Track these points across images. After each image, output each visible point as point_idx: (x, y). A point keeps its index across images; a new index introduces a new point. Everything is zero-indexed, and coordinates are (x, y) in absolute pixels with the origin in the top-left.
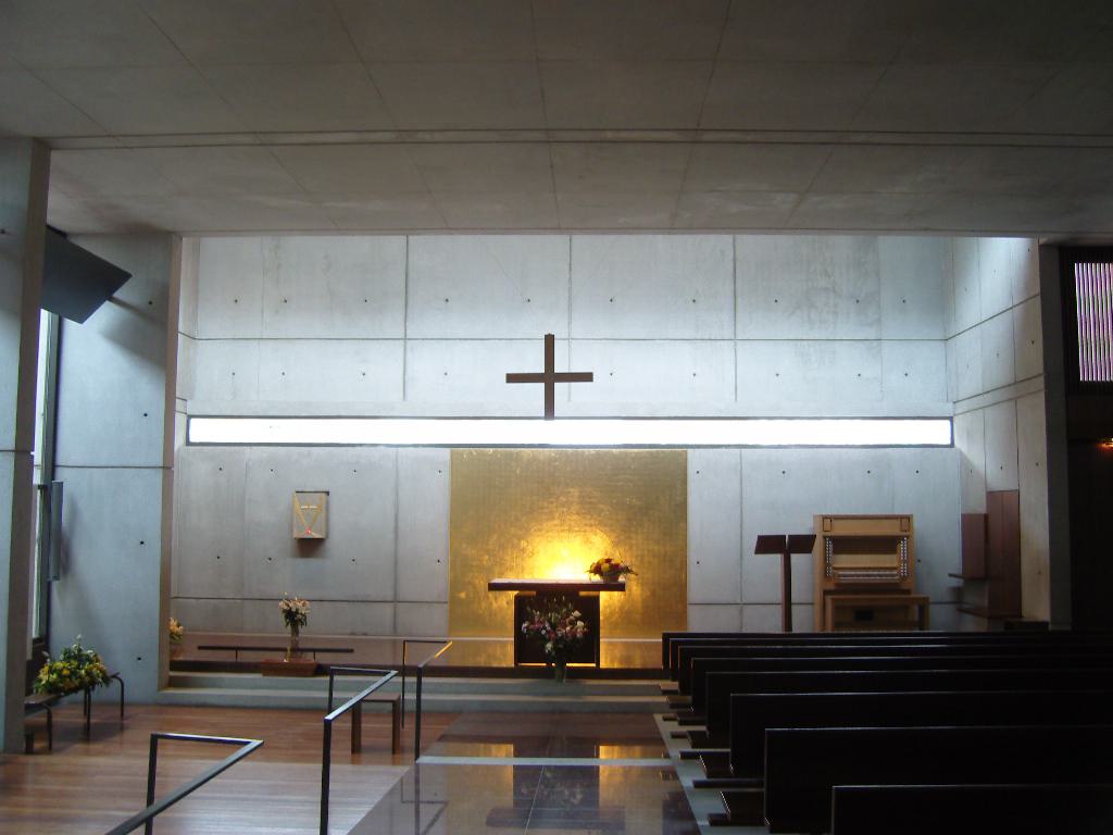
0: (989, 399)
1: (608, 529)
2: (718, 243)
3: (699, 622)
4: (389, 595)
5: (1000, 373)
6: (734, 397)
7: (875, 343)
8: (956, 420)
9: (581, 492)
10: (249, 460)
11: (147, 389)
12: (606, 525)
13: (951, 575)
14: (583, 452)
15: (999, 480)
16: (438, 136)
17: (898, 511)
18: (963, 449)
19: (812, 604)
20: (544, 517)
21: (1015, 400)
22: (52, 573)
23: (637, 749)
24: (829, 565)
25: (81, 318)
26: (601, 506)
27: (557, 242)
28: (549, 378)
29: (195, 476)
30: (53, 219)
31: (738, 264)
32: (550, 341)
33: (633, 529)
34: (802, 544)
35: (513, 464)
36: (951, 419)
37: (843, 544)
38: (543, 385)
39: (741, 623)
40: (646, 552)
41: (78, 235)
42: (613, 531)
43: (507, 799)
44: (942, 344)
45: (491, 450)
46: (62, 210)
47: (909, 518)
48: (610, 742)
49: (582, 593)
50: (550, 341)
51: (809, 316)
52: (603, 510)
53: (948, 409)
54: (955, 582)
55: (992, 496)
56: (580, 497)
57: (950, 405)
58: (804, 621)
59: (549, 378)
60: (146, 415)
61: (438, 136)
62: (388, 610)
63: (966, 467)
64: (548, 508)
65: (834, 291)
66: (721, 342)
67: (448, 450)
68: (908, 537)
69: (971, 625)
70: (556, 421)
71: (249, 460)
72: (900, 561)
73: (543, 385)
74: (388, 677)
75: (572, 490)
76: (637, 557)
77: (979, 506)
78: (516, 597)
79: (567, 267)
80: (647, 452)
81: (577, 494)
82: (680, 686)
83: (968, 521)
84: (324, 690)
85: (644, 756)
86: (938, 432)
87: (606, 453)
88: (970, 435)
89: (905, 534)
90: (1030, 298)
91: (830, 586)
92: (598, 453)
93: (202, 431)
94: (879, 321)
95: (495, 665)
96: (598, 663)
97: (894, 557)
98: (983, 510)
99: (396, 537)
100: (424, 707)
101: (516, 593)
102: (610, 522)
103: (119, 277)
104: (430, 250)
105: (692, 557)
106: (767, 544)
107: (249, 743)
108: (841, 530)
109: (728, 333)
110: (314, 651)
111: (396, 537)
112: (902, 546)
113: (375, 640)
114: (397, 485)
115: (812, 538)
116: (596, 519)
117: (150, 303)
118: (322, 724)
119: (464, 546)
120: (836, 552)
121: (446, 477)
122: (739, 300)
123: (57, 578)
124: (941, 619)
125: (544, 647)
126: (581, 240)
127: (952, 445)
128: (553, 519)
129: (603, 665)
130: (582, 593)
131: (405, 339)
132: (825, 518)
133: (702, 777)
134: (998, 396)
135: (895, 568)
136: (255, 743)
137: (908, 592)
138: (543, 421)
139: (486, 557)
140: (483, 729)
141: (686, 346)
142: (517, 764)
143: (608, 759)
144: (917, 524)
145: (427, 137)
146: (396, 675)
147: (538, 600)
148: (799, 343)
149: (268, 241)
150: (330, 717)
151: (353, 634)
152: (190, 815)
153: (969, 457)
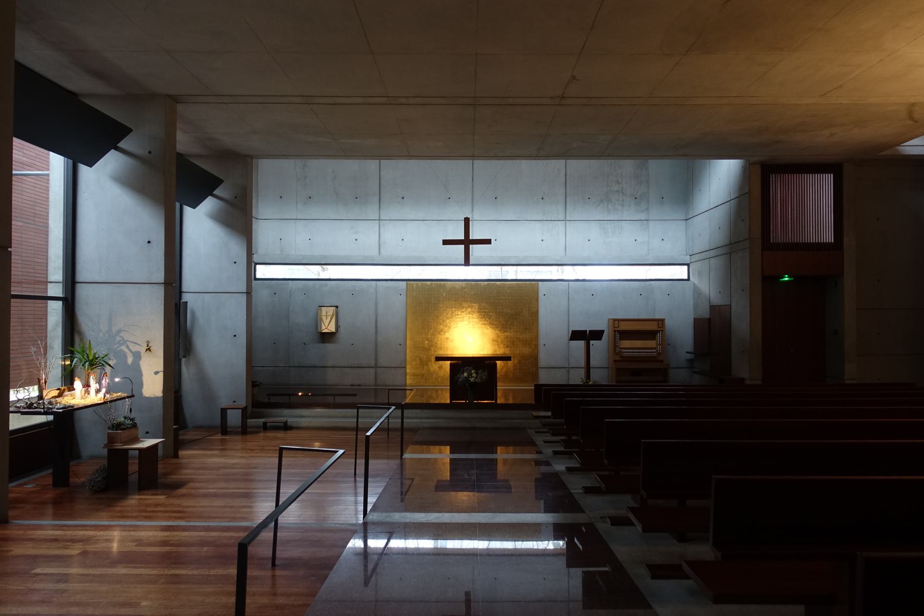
0: (712, 253)
1: (494, 326)
2: (558, 165)
3: (545, 378)
4: (373, 363)
5: (720, 238)
6: (564, 253)
7: (645, 222)
8: (691, 265)
9: (479, 306)
10: (292, 288)
11: (237, 248)
12: (493, 324)
13: (687, 352)
14: (480, 284)
15: (717, 300)
16: (412, 101)
17: (657, 317)
18: (695, 282)
19: (608, 368)
20: (459, 320)
21: (730, 253)
22: (181, 354)
23: (511, 449)
24: (617, 346)
25: (194, 206)
26: (491, 314)
27: (466, 164)
28: (467, 242)
29: (262, 295)
30: (180, 148)
31: (567, 178)
32: (467, 221)
33: (508, 326)
34: (597, 335)
35: (442, 290)
36: (688, 265)
37: (625, 335)
38: (463, 246)
39: (569, 378)
40: (515, 340)
41: (190, 156)
42: (497, 327)
43: (447, 475)
44: (684, 222)
45: (429, 282)
46: (184, 143)
47: (663, 320)
48: (506, 444)
49: (487, 362)
50: (467, 221)
51: (607, 207)
52: (491, 316)
53: (687, 259)
54: (689, 356)
55: (712, 307)
56: (478, 308)
57: (688, 257)
58: (599, 376)
59: (467, 242)
60: (235, 263)
61: (412, 101)
62: (372, 371)
63: (696, 291)
64: (461, 315)
65: (623, 193)
66: (557, 222)
67: (405, 282)
68: (662, 331)
69: (697, 380)
70: (471, 267)
71: (292, 288)
72: (657, 344)
73: (463, 246)
74: (391, 410)
75: (474, 305)
76: (510, 341)
77: (705, 313)
78: (450, 364)
79: (471, 180)
80: (516, 284)
81: (477, 307)
82: (552, 414)
83: (697, 322)
84: (353, 417)
85: (514, 453)
86: (680, 272)
87: (493, 284)
88: (700, 274)
89: (661, 329)
90: (741, 195)
91: (617, 358)
92: (488, 284)
93: (262, 272)
94: (647, 209)
95: (432, 402)
96: (496, 401)
97: (654, 342)
98: (707, 316)
99: (376, 332)
100: (405, 426)
101: (449, 362)
102: (496, 322)
103: (217, 182)
104: (394, 169)
105: (541, 342)
106: (576, 335)
107: (338, 451)
108: (624, 327)
109: (561, 217)
110: (334, 395)
111: (376, 332)
112: (659, 336)
113: (381, 389)
114: (376, 304)
115: (602, 332)
116: (487, 321)
117: (236, 197)
118: (365, 437)
119: (509, 334)
120: (621, 339)
121: (403, 297)
122: (568, 198)
123: (184, 357)
124: (679, 376)
125: (118, 382)
126: (480, 164)
127: (688, 279)
128: (464, 320)
129: (499, 402)
130: (487, 362)
131: (380, 220)
132: (615, 320)
133: (575, 464)
134: (719, 252)
135: (654, 348)
136: (341, 452)
137: (662, 361)
138: (463, 267)
139: (427, 342)
140: (431, 438)
141: (538, 225)
142: (498, 461)
143: (502, 454)
144: (668, 323)
145: (404, 101)
146: (395, 408)
147: (460, 364)
148: (601, 222)
149: (299, 162)
150: (368, 434)
151: (352, 385)
152: (343, 498)
153: (699, 286)
